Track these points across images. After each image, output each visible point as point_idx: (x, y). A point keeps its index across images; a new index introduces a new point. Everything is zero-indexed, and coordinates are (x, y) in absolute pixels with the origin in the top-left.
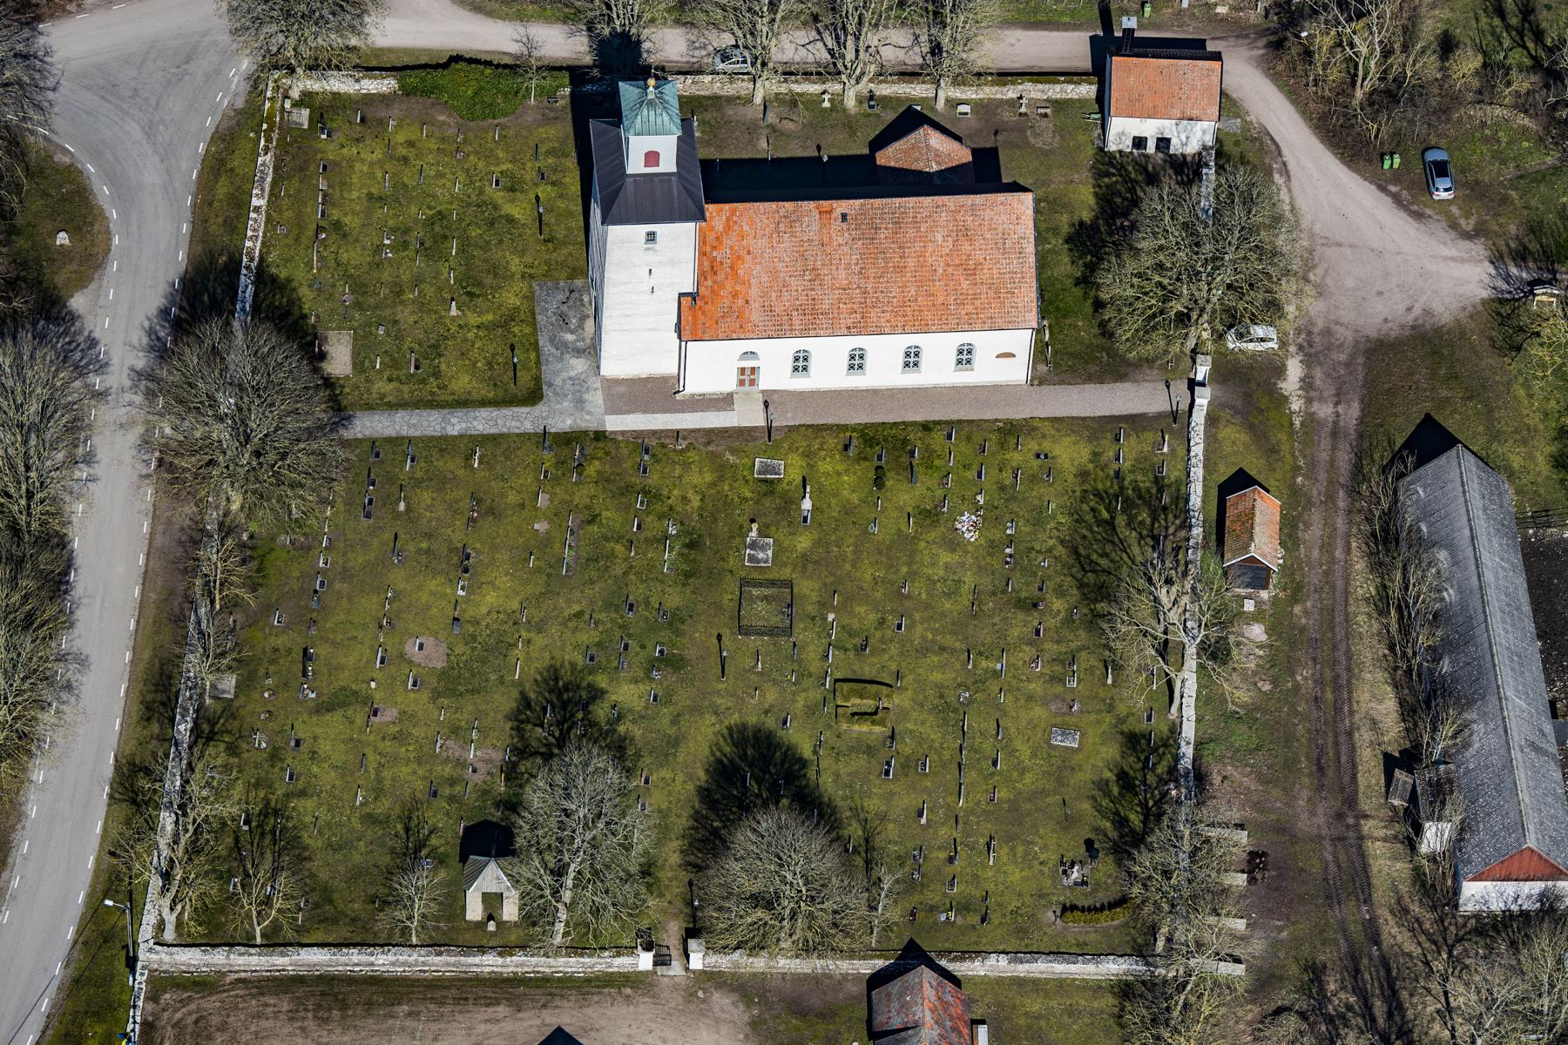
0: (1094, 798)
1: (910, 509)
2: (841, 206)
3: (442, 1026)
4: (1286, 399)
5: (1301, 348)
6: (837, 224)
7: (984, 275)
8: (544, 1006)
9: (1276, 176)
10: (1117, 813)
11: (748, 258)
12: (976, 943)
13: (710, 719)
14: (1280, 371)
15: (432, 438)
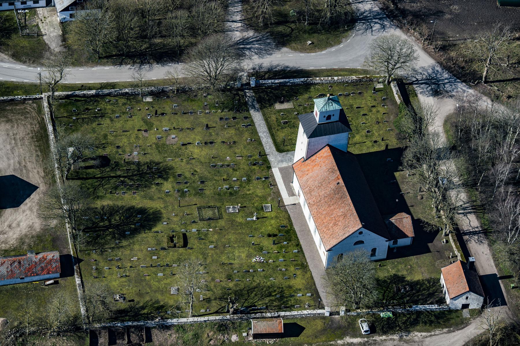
0: (151, 300)
1: (261, 244)
2: (341, 181)
3: (35, 162)
4: (342, 339)
5: (368, 342)
6: (336, 183)
7: (335, 228)
8: (46, 183)
9: (447, 329)
10: (146, 306)
11: (319, 167)
12: (85, 276)
13: (162, 206)
14: (355, 336)
15: (256, 130)
